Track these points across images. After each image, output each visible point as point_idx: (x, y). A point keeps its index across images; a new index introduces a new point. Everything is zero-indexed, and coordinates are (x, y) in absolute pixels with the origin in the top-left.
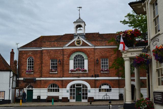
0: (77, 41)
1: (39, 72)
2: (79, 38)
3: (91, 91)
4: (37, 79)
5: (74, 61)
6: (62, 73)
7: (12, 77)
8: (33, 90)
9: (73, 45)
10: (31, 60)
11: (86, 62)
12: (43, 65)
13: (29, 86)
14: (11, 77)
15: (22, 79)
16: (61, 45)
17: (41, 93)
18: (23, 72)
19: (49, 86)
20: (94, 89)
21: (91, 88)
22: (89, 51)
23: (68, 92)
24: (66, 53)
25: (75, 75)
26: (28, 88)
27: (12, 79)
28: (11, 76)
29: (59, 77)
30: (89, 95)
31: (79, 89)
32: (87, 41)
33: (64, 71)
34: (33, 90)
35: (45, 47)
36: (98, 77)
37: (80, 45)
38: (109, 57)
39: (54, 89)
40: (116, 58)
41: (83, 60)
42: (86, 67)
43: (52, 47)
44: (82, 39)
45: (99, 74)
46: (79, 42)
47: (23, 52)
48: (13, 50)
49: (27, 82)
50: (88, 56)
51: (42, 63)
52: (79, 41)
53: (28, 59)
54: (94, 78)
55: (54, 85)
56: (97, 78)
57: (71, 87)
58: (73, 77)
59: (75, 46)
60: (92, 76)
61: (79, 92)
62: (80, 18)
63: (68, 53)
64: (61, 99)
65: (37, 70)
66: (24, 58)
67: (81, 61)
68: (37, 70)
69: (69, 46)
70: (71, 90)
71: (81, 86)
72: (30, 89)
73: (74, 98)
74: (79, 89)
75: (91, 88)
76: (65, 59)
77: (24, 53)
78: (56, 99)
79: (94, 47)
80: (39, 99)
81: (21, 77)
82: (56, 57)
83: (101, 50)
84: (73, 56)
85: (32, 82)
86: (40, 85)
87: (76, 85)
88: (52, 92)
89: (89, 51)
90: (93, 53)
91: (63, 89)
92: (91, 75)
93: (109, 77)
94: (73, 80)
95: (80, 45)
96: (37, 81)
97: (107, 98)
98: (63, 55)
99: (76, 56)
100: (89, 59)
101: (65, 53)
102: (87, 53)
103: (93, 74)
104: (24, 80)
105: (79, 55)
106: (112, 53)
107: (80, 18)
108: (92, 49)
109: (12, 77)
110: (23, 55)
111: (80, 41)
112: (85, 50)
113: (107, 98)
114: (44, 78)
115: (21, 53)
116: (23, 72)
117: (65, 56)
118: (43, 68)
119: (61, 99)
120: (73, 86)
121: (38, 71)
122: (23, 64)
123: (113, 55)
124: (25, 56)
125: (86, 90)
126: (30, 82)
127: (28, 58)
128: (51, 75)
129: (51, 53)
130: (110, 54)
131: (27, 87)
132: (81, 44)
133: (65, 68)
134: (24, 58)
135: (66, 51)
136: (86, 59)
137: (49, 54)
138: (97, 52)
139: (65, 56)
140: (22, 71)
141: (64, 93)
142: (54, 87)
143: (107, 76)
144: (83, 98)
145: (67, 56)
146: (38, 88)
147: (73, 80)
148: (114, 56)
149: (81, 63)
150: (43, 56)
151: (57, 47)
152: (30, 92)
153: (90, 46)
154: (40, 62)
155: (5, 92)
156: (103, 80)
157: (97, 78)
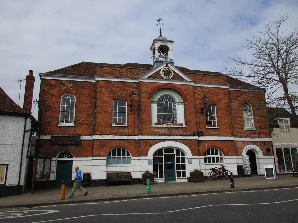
1: (88, 124)
2: (167, 66)
3: (194, 161)
4: (83, 138)
5: (159, 105)
7: (28, 131)
8: (72, 161)
9: (157, 76)
10: (68, 99)
12: (98, 109)
13: (62, 154)
14: (277, 63)
15: (49, 138)
17: (97, 167)
18: (49, 123)
19: (110, 153)
20: (198, 157)
21: (193, 155)
22: (185, 90)
23: (150, 164)
24: (145, 90)
25: (163, 131)
26: (59, 157)
27: (28, 134)
28: (27, 129)
30: (189, 169)
31: (169, 158)
33: (140, 122)
34: (72, 161)
35: (103, 76)
36: (202, 135)
38: (217, 103)
39: (213, 158)
40: (227, 104)
42: (180, 118)
43: (116, 77)
45: (203, 130)
47: (53, 83)
48: (31, 72)
49: (59, 144)
50: (184, 99)
51: (95, 105)
52: (169, 71)
54: (196, 138)
55: (119, 150)
56: (201, 138)
57: (155, 154)
59: (161, 78)
60: (194, 135)
61: (169, 163)
62: (161, 36)
63: (148, 90)
64: (141, 178)
65: (83, 119)
66: (53, 95)
67: (163, 110)
68: (83, 119)
69: (150, 77)
70: (155, 160)
72: (65, 159)
73: (161, 176)
74: (169, 158)
75: (264, 155)
77: (55, 85)
78: (125, 180)
79: (193, 84)
80: (87, 181)
81: (45, 134)
82: (124, 95)
83: (203, 90)
84: (157, 97)
85: (72, 145)
86: (91, 150)
87: (164, 149)
88: (211, 162)
89: (185, 90)
90: (192, 94)
91: (141, 157)
92: (192, 131)
93: (220, 135)
94: (160, 141)
96: (82, 142)
97: (55, 166)
98: (140, 93)
99: (162, 97)
100: (186, 103)
101: (144, 90)
103: (194, 130)
104: (53, 139)
105: (166, 96)
106: (220, 97)
108: (191, 87)
109: (30, 132)
110: (52, 89)
112: (180, 87)
113: (55, 166)
114: (101, 135)
115: (45, 84)
116: (49, 123)
117: (143, 96)
118: (98, 116)
119: (141, 178)
120: (160, 151)
121: (85, 122)
122: (50, 106)
123: (223, 99)
124: (55, 90)
125: (183, 160)
126: (64, 145)
129: (114, 88)
130: (218, 98)
131: (57, 156)
132: (172, 76)
133: (144, 117)
134: (53, 95)
135: (145, 86)
136: (179, 103)
137: (109, 89)
138: (198, 93)
139: (143, 96)
140: (49, 120)
141: (139, 166)
142: (213, 154)
144: (179, 176)
145: (147, 95)
146: (84, 157)
147: (160, 141)
148: (224, 101)
150: (98, 93)
152: (65, 168)
153: (187, 81)
154: (89, 104)
155: (9, 166)
156: (210, 141)
157: (201, 138)
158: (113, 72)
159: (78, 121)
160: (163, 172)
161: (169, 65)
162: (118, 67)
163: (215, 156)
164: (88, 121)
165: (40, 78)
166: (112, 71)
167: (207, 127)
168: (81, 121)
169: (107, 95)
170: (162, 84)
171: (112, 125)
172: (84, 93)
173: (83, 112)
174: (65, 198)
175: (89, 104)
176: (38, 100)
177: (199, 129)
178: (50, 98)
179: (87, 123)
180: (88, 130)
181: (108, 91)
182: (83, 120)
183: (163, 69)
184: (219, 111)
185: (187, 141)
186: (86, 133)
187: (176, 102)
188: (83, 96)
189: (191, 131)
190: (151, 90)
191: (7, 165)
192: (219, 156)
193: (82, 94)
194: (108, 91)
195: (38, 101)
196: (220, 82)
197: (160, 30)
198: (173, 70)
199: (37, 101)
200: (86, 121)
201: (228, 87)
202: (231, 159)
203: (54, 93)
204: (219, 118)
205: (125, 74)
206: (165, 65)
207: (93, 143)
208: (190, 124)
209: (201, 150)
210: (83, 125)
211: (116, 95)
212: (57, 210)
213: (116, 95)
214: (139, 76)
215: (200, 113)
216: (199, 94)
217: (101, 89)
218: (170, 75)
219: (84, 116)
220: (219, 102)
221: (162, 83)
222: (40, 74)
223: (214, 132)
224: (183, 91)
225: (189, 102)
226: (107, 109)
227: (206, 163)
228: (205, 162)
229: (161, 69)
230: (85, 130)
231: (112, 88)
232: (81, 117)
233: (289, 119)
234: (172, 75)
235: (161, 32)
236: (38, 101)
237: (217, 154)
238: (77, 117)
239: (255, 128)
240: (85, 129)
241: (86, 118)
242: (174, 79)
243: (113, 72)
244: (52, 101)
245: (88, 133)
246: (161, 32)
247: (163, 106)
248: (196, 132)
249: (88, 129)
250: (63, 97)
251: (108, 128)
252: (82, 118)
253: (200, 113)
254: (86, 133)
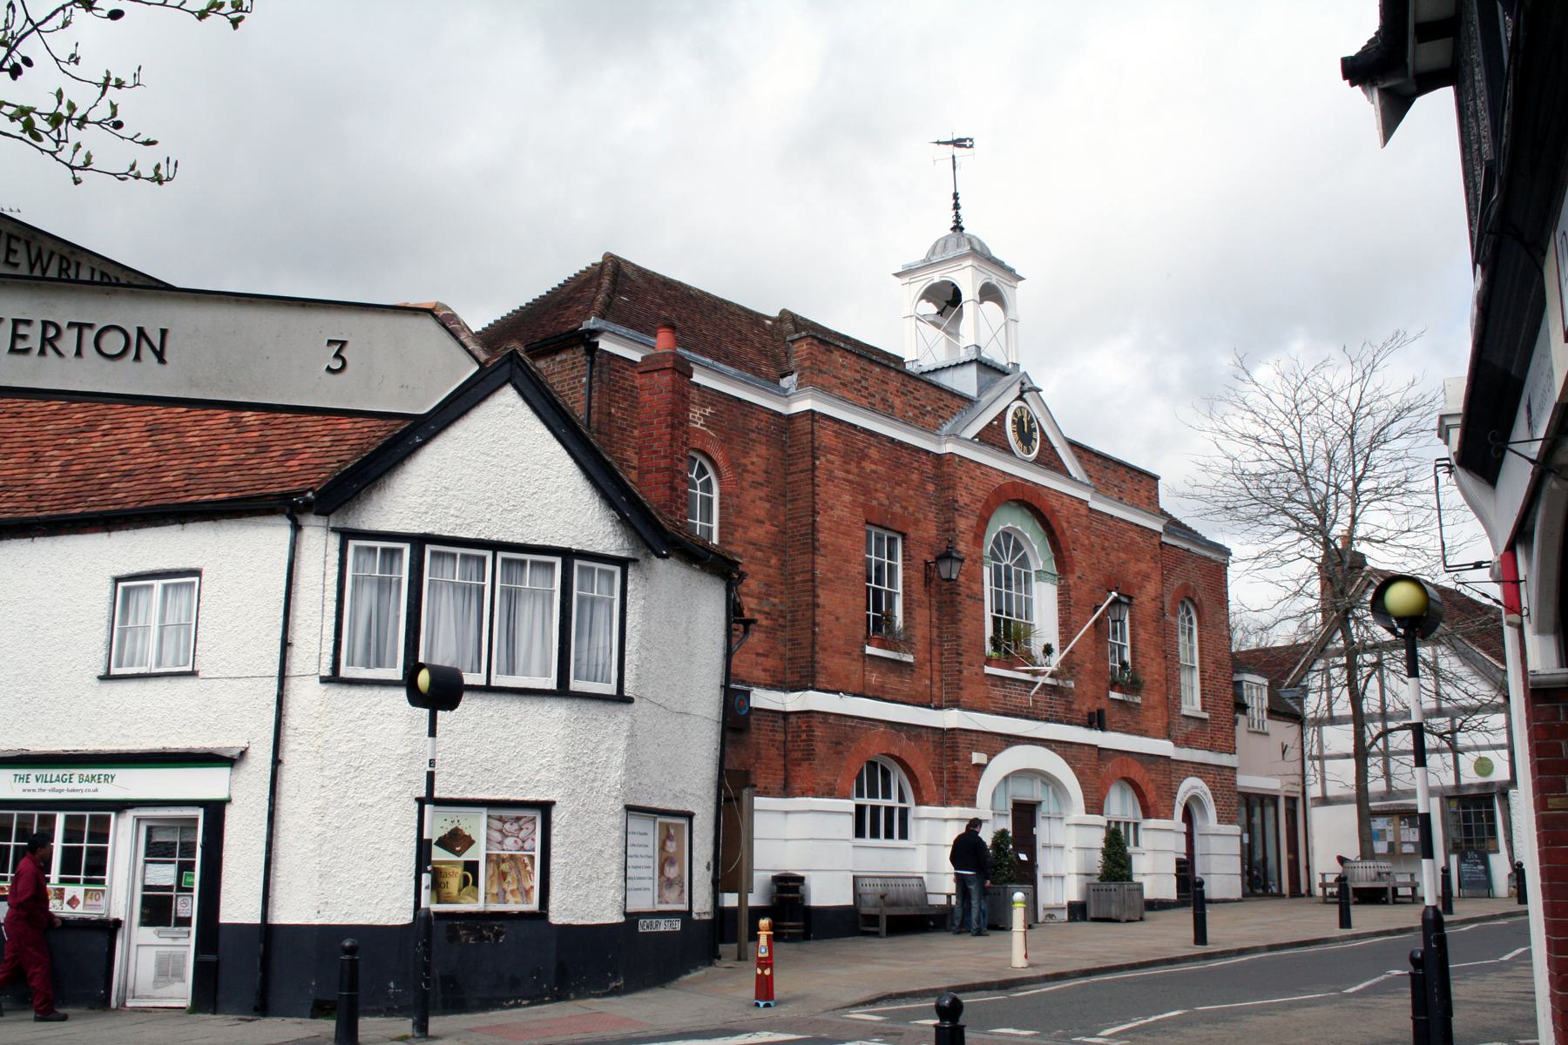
50: (1063, 562)
59: (1007, 449)
62: (958, 227)
107: (958, 227)
112: (1055, 504)
142: (873, 794)
151: (908, 422)
154: (767, 526)
155: (557, 816)
161: (1026, 396)
162: (878, 364)
163: (880, 802)
167: (870, 650)
170: (1008, 480)
172: (750, 467)
185: (1074, 749)
187: (1034, 568)
191: (545, 808)
192: (894, 802)
197: (956, 196)
201: (1160, 529)
202: (823, 816)
207: (810, 730)
211: (875, 503)
212: (780, 1031)
223: (892, 681)
227: (860, 841)
228: (859, 833)
235: (956, 207)
237: (887, 795)
239: (1204, 709)
240: (758, 655)
246: (956, 207)
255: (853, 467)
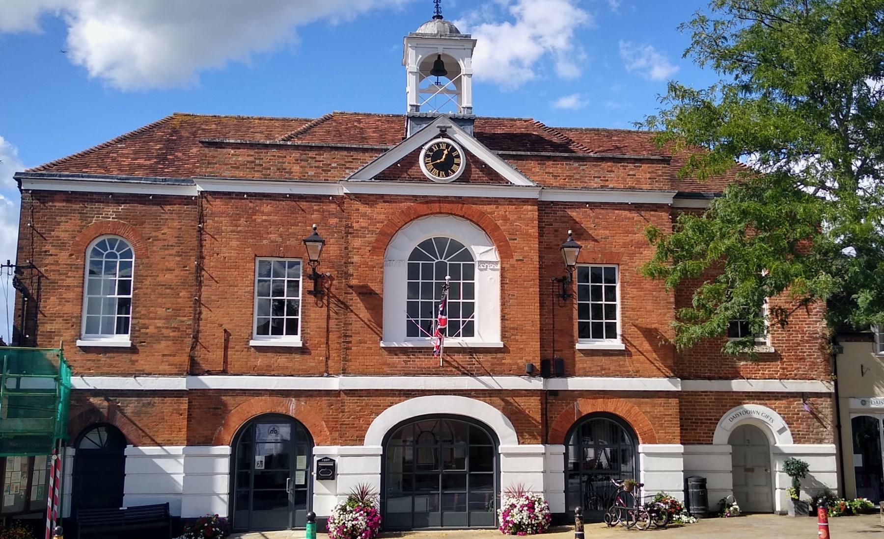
0: (430, 149)
1: (175, 340)
2: (443, 133)
6: (333, 345)
9: (403, 170)
11: (487, 288)
16: (326, 169)
24: (363, 223)
29: (236, 372)
32: (503, 157)
37: (453, 177)
38: (625, 258)
41: (469, 273)
43: (266, 178)
44: (464, 139)
46: (443, 161)
53: (95, 252)
56: (556, 384)
58: (406, 375)
65: (160, 323)
66: (62, 246)
68: (160, 323)
69: (382, 177)
71: (255, 492)
76: (356, 259)
95: (453, 177)
102: (497, 228)
110: (59, 223)
111: (456, 160)
116: (51, 335)
121: (164, 331)
127: (93, 245)
128: (260, 361)
129: (259, 218)
130: (628, 239)
132: (459, 171)
137: (242, 221)
138: (556, 225)
139: (357, 243)
140: (48, 327)
143: (612, 368)
145: (371, 238)
149: (427, 274)
154: (177, 272)
157: (556, 384)
158: (257, 162)
159: (143, 331)
160: (492, 475)
164: (175, 329)
165: (20, 186)
166: (252, 159)
168: (151, 330)
169: (234, 243)
171: (252, 343)
172: (161, 237)
173: (160, 300)
174: (545, 460)
175: (177, 272)
176: (13, 262)
177: (550, 351)
178: (51, 255)
179: (172, 334)
180: (177, 359)
181: (239, 228)
182: (158, 325)
183: (427, 147)
184: (629, 289)
186: (165, 367)
188: (159, 244)
189: (519, 361)
190: (386, 222)
193: (156, 239)
194: (239, 228)
195: (12, 266)
196: (639, 182)
198: (463, 148)
199: (9, 265)
200: (167, 328)
203: (64, 236)
204: (628, 314)
205: (296, 168)
206: (438, 132)
208: (517, 337)
209: (553, 425)
210: (158, 341)
213: (265, 242)
214: (347, 171)
215: (559, 296)
216: (556, 231)
217: (217, 222)
218: (454, 167)
219: (161, 312)
220: (632, 256)
221: (423, 196)
222: (17, 174)
224: (499, 223)
225: (517, 260)
226: (236, 289)
229: (421, 148)
230: (165, 359)
231: (254, 217)
232: (151, 315)
233: (256, 468)
234: (458, 165)
236: (12, 266)
238: (138, 315)
240: (164, 355)
241: (167, 318)
242: (465, 178)
243: (257, 162)
244: (57, 263)
245: (176, 371)
247: (427, 274)
248: (538, 365)
249: (174, 356)
250: (94, 249)
251: (237, 351)
252: (155, 319)
253: (559, 296)
254: (165, 367)
255: (242, 221)
